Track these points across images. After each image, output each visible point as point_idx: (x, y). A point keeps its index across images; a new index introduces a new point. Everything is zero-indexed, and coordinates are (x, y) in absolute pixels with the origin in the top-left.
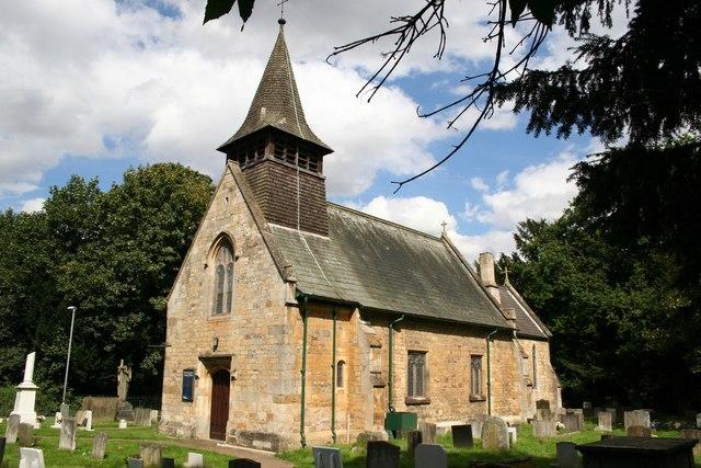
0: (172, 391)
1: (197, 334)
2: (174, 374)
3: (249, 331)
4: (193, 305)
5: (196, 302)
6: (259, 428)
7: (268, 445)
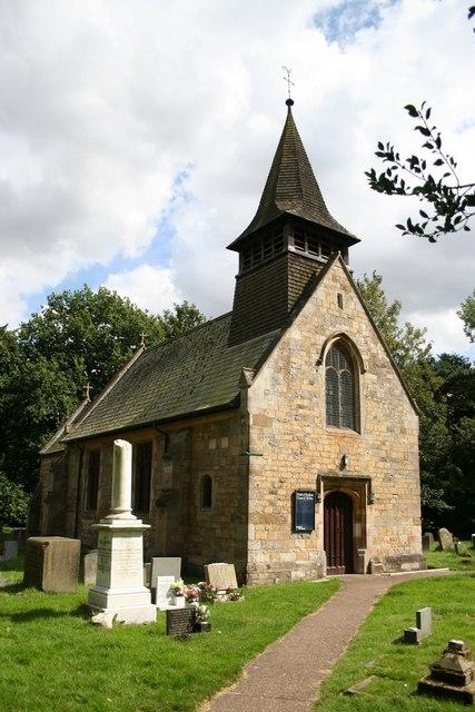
0: (266, 519)
1: (312, 446)
2: (272, 497)
3: (383, 454)
4: (300, 407)
5: (306, 403)
6: (403, 552)
7: (417, 565)
